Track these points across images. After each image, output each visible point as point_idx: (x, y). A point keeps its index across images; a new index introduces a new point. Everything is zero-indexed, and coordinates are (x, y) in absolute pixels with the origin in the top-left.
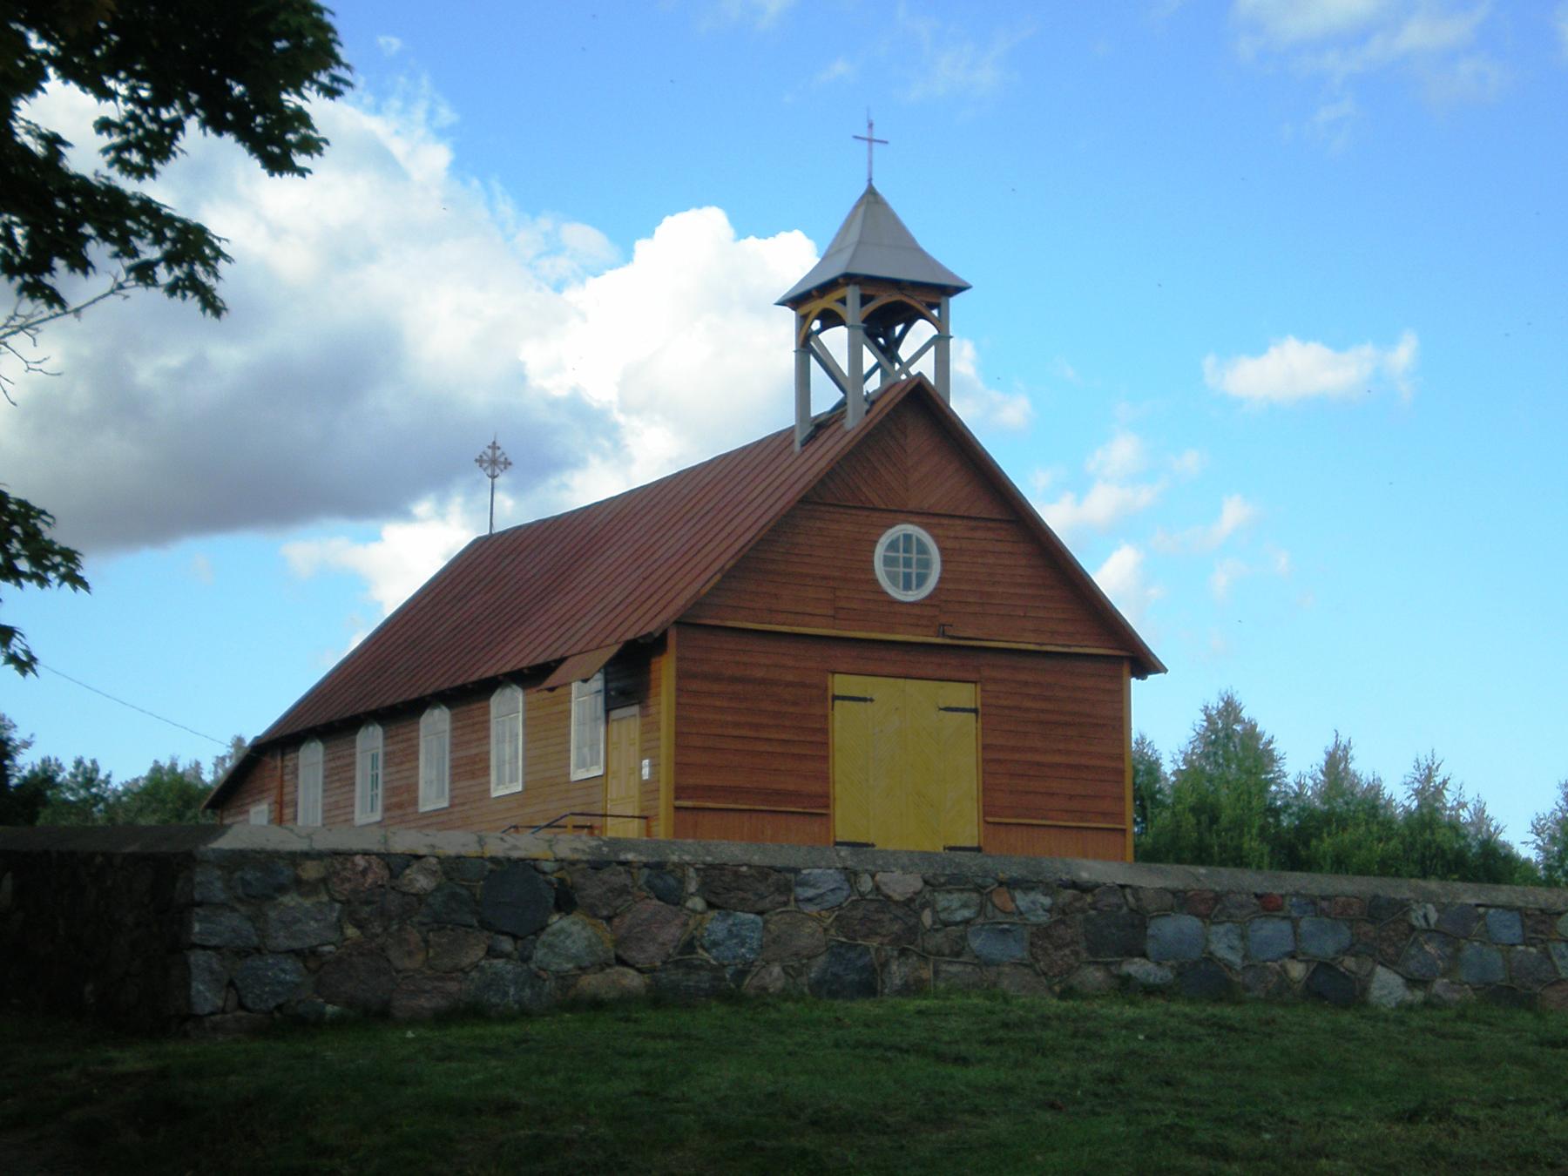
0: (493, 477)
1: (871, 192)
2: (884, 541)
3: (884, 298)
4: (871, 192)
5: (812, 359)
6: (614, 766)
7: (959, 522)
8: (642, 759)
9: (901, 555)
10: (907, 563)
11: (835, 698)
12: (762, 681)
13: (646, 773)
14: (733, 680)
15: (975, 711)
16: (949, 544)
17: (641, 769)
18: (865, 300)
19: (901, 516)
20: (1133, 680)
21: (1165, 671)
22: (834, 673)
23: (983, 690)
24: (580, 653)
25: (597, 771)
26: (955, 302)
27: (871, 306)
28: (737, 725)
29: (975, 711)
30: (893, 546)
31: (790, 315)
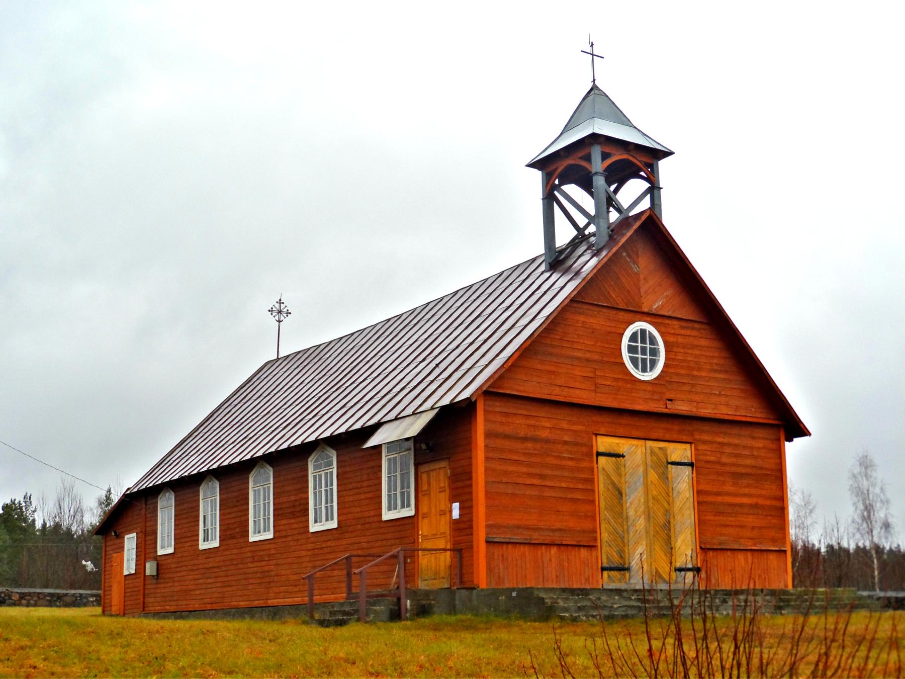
0: (279, 321)
1: (594, 88)
2: (628, 334)
3: (618, 156)
4: (594, 88)
5: (556, 206)
6: (424, 509)
7: (675, 322)
8: (452, 501)
9: (639, 345)
10: (644, 352)
11: (599, 454)
12: (547, 441)
13: (456, 514)
14: (525, 439)
15: (691, 464)
16: (671, 339)
17: (451, 512)
18: (605, 156)
19: (639, 316)
20: (787, 444)
21: (810, 434)
22: (596, 435)
23: (696, 449)
24: (396, 419)
25: (409, 512)
26: (663, 165)
27: (609, 162)
28: (530, 475)
29: (691, 464)
30: (633, 338)
31: (537, 175)
